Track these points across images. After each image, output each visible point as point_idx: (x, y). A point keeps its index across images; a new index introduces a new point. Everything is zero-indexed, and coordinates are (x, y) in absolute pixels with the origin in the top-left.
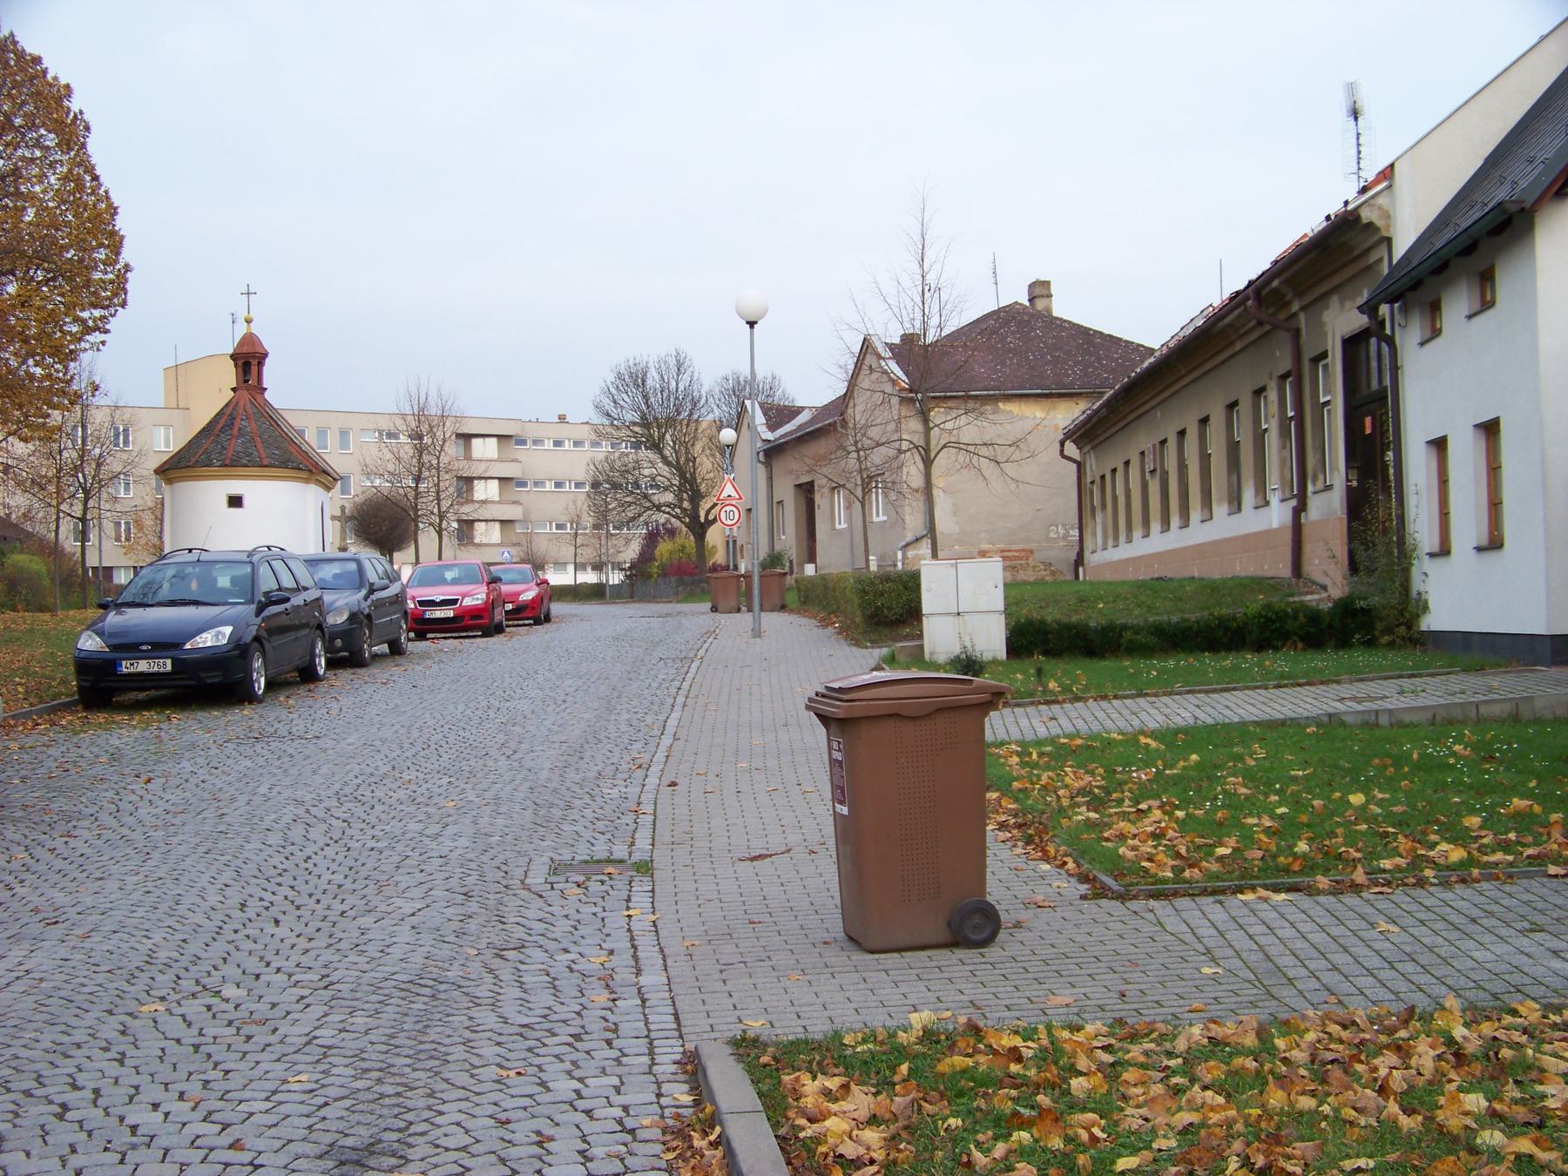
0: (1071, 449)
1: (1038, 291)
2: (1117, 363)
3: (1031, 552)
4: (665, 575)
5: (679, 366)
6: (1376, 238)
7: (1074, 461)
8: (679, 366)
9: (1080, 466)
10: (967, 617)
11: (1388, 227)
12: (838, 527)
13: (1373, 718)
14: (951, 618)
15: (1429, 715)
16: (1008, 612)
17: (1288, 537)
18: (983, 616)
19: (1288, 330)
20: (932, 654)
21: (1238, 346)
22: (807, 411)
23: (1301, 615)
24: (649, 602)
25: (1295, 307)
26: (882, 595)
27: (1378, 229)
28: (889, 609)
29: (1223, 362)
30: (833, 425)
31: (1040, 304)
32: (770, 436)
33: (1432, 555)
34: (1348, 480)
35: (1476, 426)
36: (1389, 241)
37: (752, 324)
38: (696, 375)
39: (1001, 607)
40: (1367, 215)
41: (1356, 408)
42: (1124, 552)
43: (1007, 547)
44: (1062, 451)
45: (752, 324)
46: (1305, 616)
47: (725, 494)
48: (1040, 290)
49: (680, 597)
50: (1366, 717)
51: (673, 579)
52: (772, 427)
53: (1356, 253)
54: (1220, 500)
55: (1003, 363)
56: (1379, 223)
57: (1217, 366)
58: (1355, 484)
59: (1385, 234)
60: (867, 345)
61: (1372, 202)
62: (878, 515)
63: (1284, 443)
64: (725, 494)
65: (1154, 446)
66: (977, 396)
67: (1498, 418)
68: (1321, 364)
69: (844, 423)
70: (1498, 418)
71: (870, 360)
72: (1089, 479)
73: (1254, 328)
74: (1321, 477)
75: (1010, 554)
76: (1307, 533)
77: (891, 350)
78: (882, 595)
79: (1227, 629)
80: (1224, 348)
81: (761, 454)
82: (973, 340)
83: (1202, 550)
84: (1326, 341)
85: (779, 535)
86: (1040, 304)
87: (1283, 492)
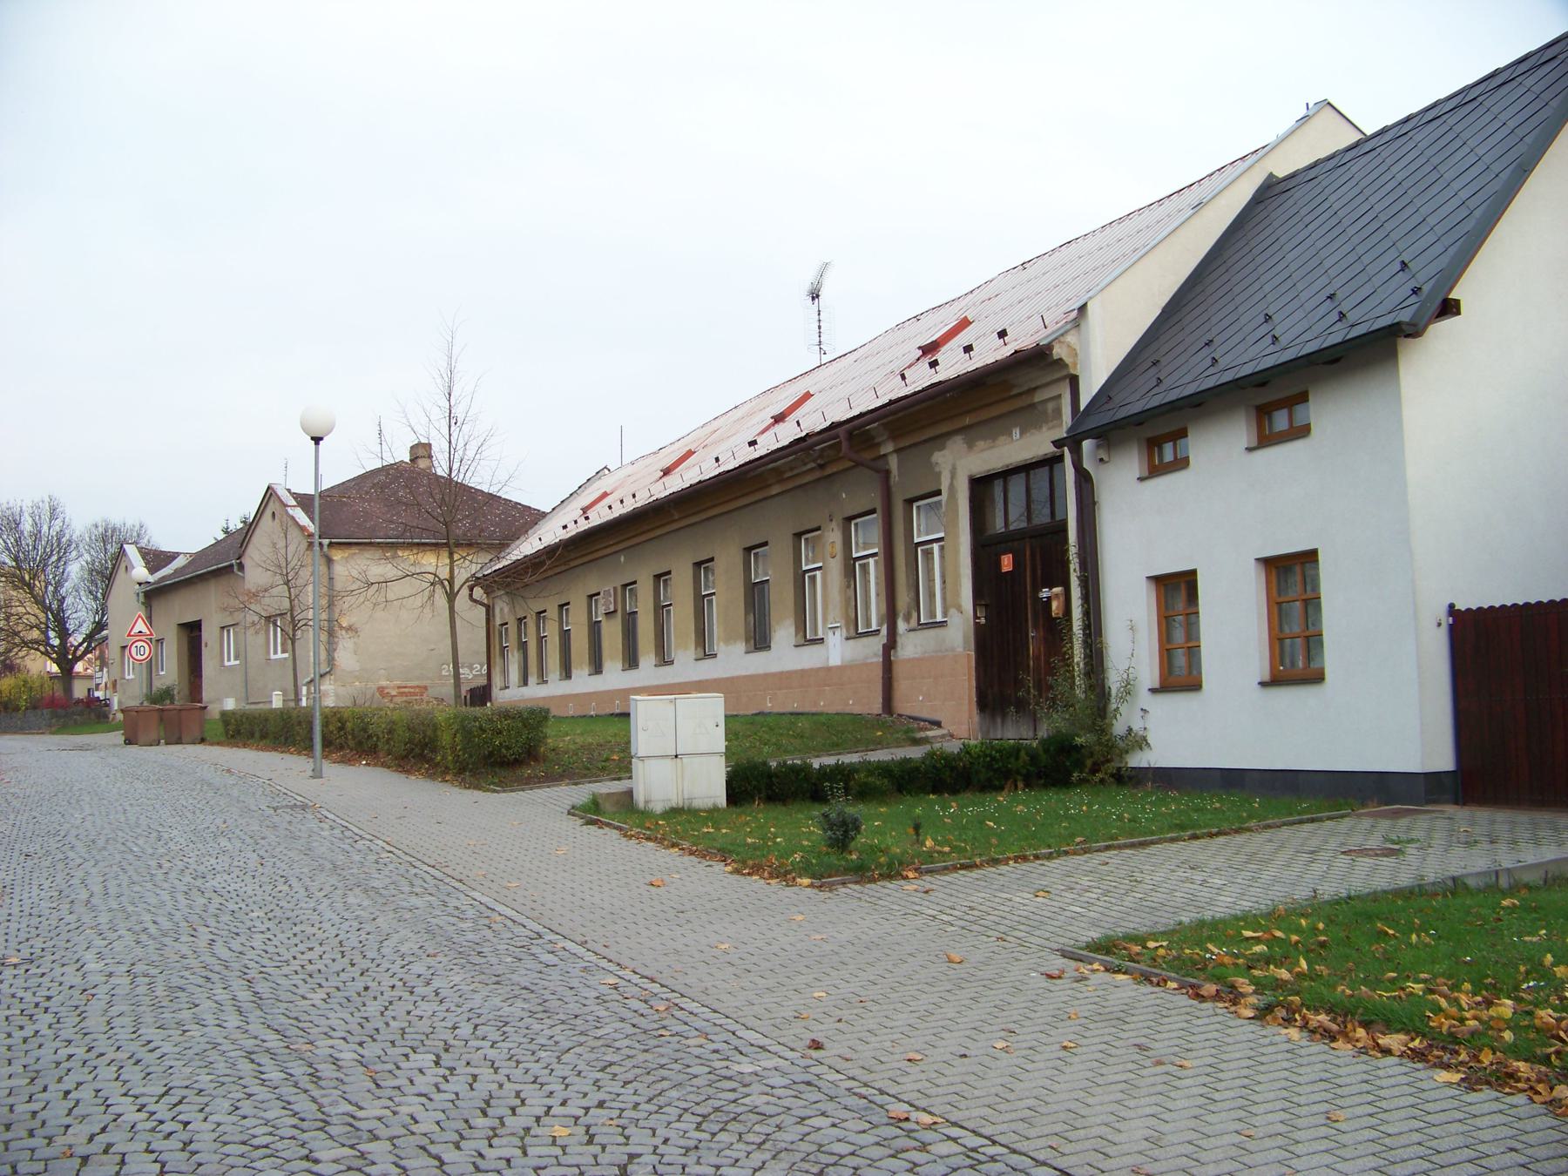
0: (478, 593)
1: (421, 452)
2: (500, 518)
3: (425, 688)
4: (35, 708)
5: (53, 510)
6: (1064, 373)
7: (482, 604)
8: (53, 510)
9: (489, 611)
10: (686, 760)
11: (1075, 364)
12: (227, 664)
13: (1494, 879)
14: (668, 762)
15: (1541, 873)
16: (729, 754)
17: (878, 673)
18: (704, 759)
19: (877, 471)
20: (646, 802)
21: (775, 490)
22: (182, 556)
23: (1023, 753)
24: (15, 733)
25: (888, 448)
26: (500, 732)
27: (1067, 366)
28: (508, 748)
29: (756, 502)
30: (231, 566)
31: (422, 464)
32: (151, 579)
33: (1153, 691)
34: (976, 617)
35: (1257, 559)
36: (1074, 381)
37: (317, 440)
38: (67, 520)
39: (721, 745)
40: (1058, 352)
41: (983, 546)
42: (535, 692)
43: (404, 684)
44: (471, 595)
45: (317, 440)
46: (1027, 754)
47: (136, 630)
48: (421, 451)
49: (53, 729)
50: (1488, 880)
51: (45, 711)
52: (152, 571)
53: (1015, 391)
54: (729, 639)
55: (398, 514)
56: (1068, 360)
57: (708, 519)
58: (983, 621)
59: (1072, 372)
60: (270, 493)
61: (1062, 339)
62: (275, 653)
63: (849, 582)
64: (136, 630)
65: (615, 589)
66: (379, 543)
67: (200, 621)
68: (915, 505)
69: (241, 567)
70: (200, 621)
71: (272, 507)
72: (498, 621)
73: (812, 470)
74: (915, 615)
75: (406, 690)
76: (898, 670)
77: (295, 499)
78: (500, 732)
79: (953, 769)
80: (761, 489)
81: (141, 595)
82: (367, 493)
83: (784, 679)
84: (940, 484)
85: (157, 670)
86: (422, 464)
87: (848, 630)
